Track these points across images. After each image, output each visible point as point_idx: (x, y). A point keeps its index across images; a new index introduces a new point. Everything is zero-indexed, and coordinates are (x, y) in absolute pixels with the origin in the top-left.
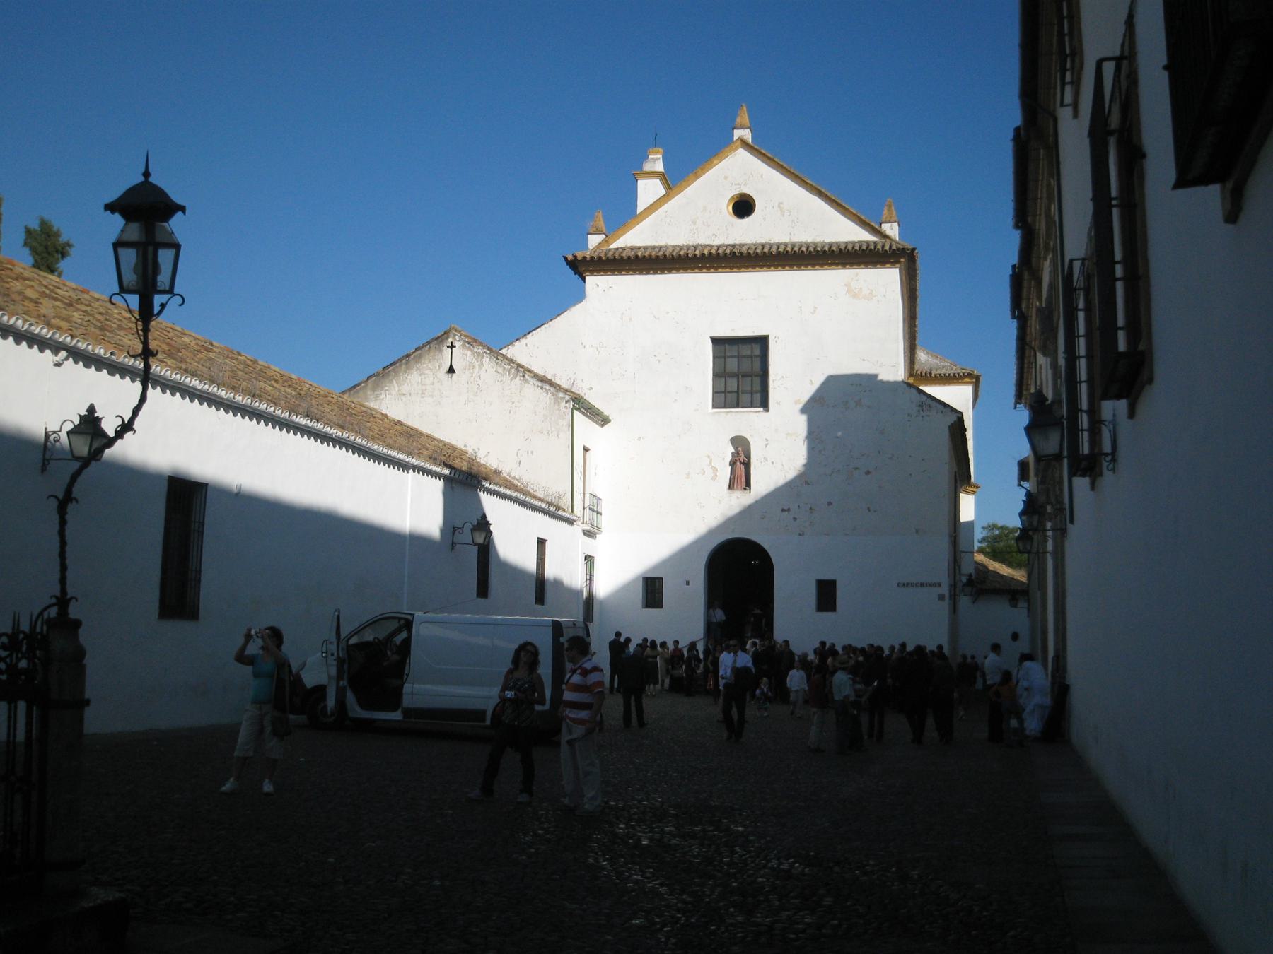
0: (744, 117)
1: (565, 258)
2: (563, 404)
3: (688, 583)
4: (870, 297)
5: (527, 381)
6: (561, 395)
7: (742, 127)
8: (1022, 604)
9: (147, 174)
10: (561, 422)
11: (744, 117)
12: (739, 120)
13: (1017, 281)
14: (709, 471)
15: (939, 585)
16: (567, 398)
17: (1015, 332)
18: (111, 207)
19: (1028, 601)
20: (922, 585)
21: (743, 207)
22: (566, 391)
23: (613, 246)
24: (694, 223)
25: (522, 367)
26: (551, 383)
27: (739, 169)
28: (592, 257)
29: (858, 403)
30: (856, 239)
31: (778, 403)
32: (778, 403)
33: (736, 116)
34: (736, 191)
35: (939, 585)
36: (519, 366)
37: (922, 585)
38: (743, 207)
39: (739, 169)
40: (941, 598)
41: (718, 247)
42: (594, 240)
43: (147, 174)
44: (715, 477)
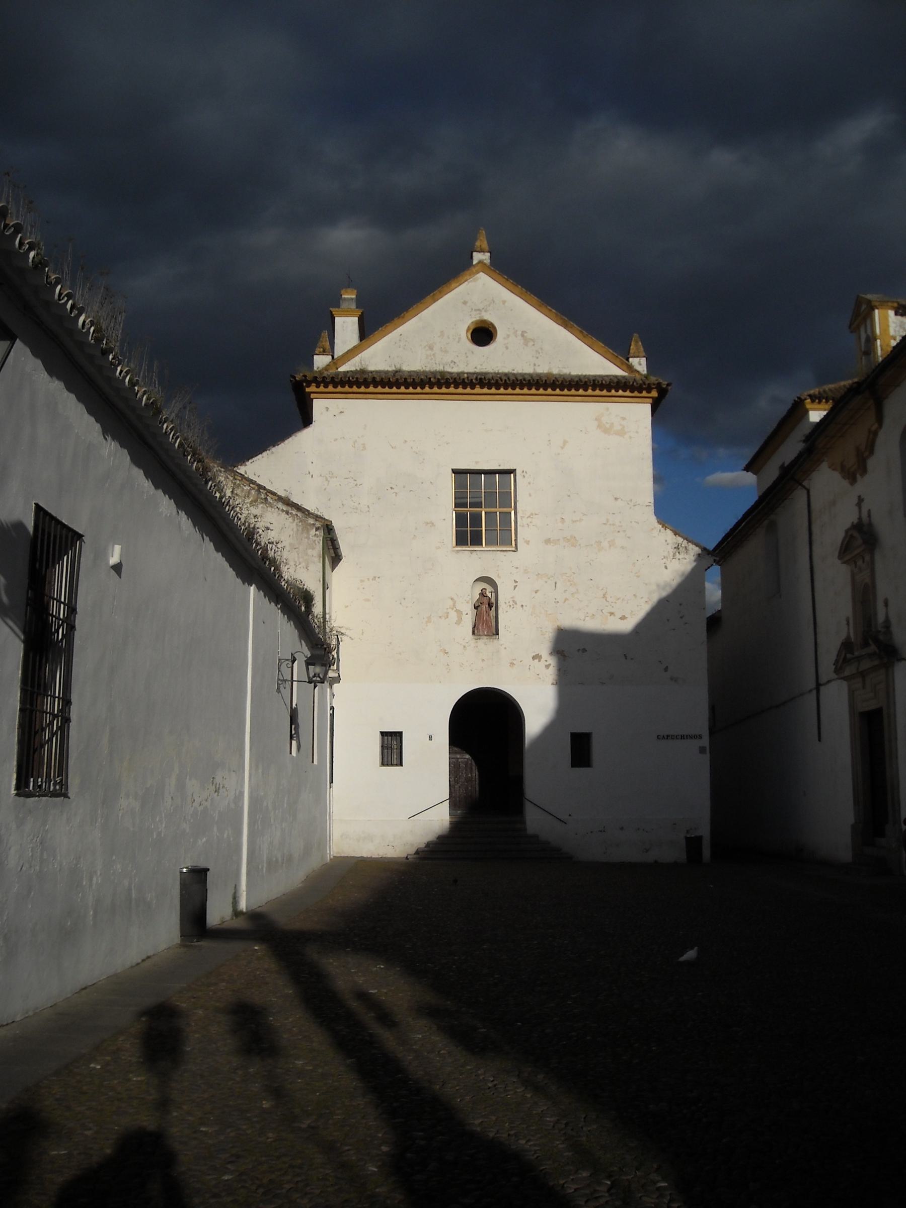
0: (482, 241)
2: (313, 532)
3: (430, 738)
4: (621, 433)
5: (271, 506)
6: (311, 521)
7: (482, 251)
10: (310, 552)
11: (482, 241)
12: (478, 244)
14: (453, 615)
15: (700, 737)
16: (318, 524)
17: (219, 560)
20: (683, 737)
21: (483, 334)
22: (317, 517)
23: (341, 369)
24: (431, 348)
25: (264, 488)
26: (298, 508)
27: (482, 292)
28: (820, 402)
29: (612, 544)
31: (528, 542)
32: (528, 542)
33: (476, 239)
34: (476, 317)
35: (700, 737)
36: (260, 487)
37: (683, 737)
38: (483, 334)
39: (482, 292)
40: (702, 750)
44: (459, 621)
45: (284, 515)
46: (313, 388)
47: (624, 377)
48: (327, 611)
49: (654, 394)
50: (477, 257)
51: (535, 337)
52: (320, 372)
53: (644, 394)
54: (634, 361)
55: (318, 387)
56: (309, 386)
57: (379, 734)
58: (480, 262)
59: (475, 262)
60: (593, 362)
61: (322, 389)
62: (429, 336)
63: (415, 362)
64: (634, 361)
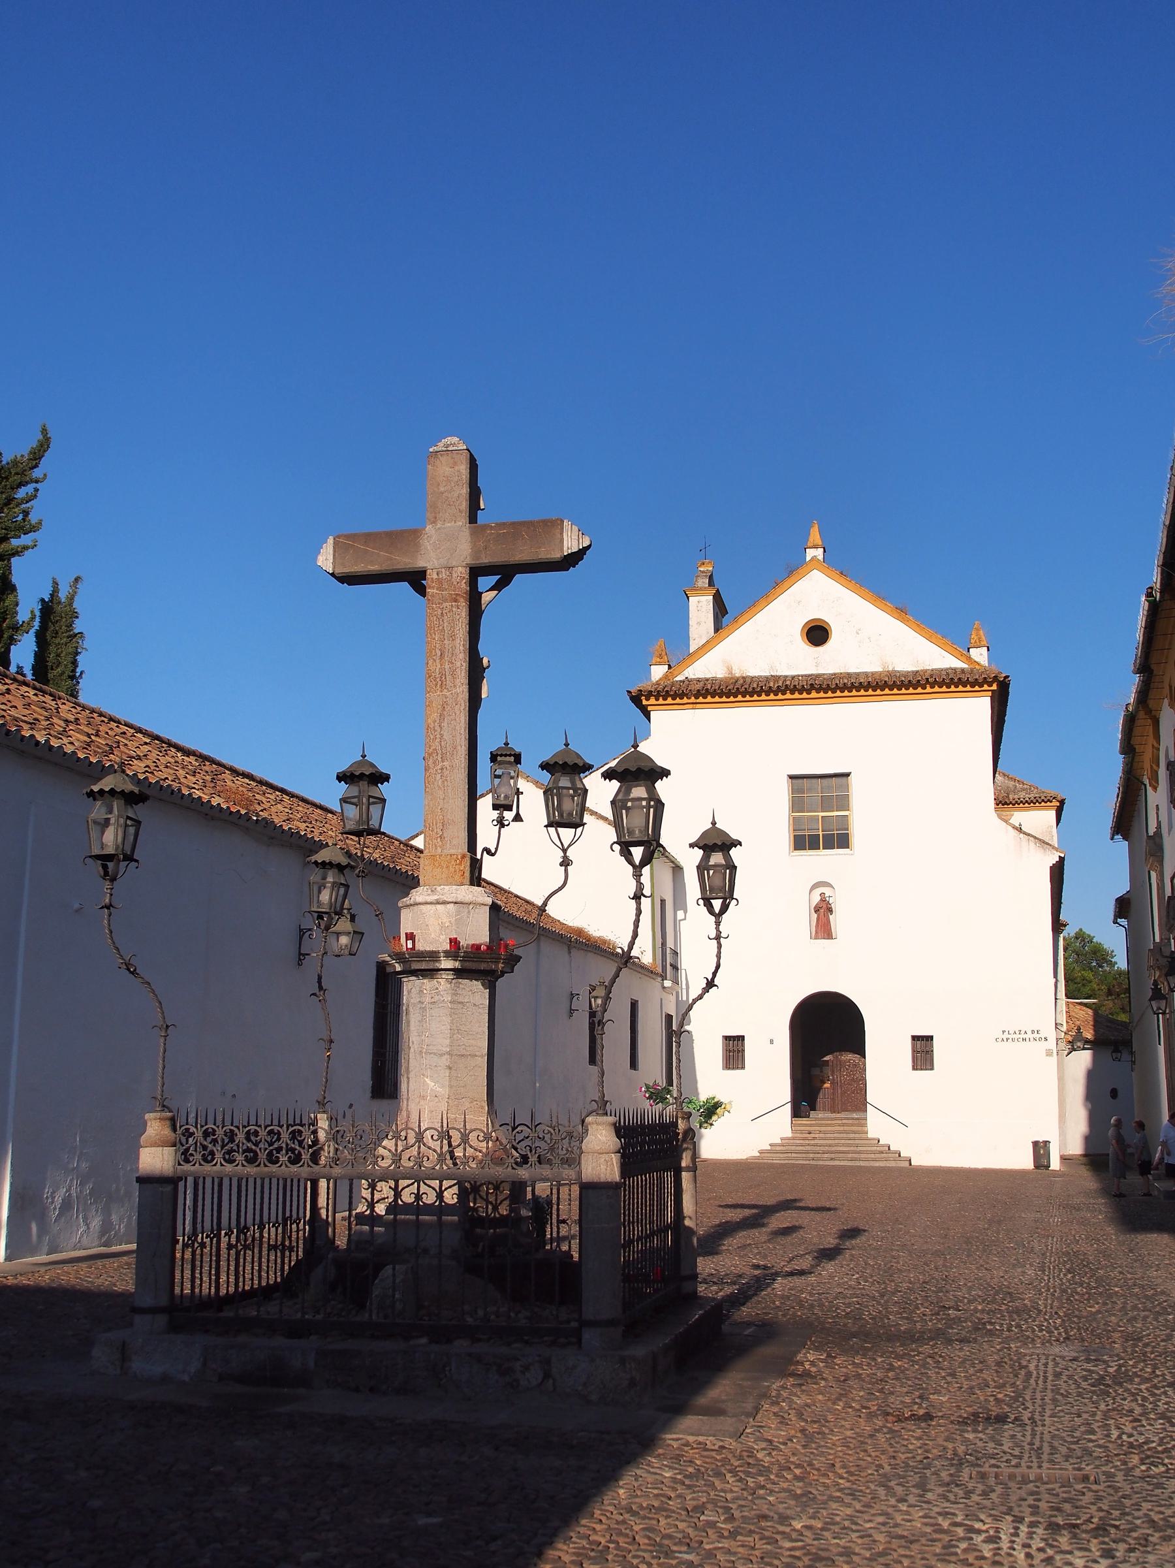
0: (815, 536)
1: (629, 692)
7: (815, 547)
8: (1125, 1056)
9: (714, 823)
11: (815, 536)
12: (811, 539)
13: (1130, 721)
18: (692, 846)
19: (1132, 1053)
23: (679, 678)
27: (816, 592)
30: (953, 666)
32: (817, 634)
39: (816, 592)
40: (1049, 1053)
41: (793, 677)
42: (658, 672)
43: (714, 823)
45: (411, 1075)
46: (652, 701)
47: (963, 671)
48: (670, 944)
49: (994, 687)
50: (810, 553)
51: (870, 635)
52: (658, 683)
53: (986, 687)
54: (975, 653)
55: (657, 700)
56: (647, 700)
57: (786, 777)
58: (814, 558)
59: (808, 559)
60: (924, 654)
61: (661, 701)
62: (765, 643)
63: (756, 667)
64: (975, 653)
